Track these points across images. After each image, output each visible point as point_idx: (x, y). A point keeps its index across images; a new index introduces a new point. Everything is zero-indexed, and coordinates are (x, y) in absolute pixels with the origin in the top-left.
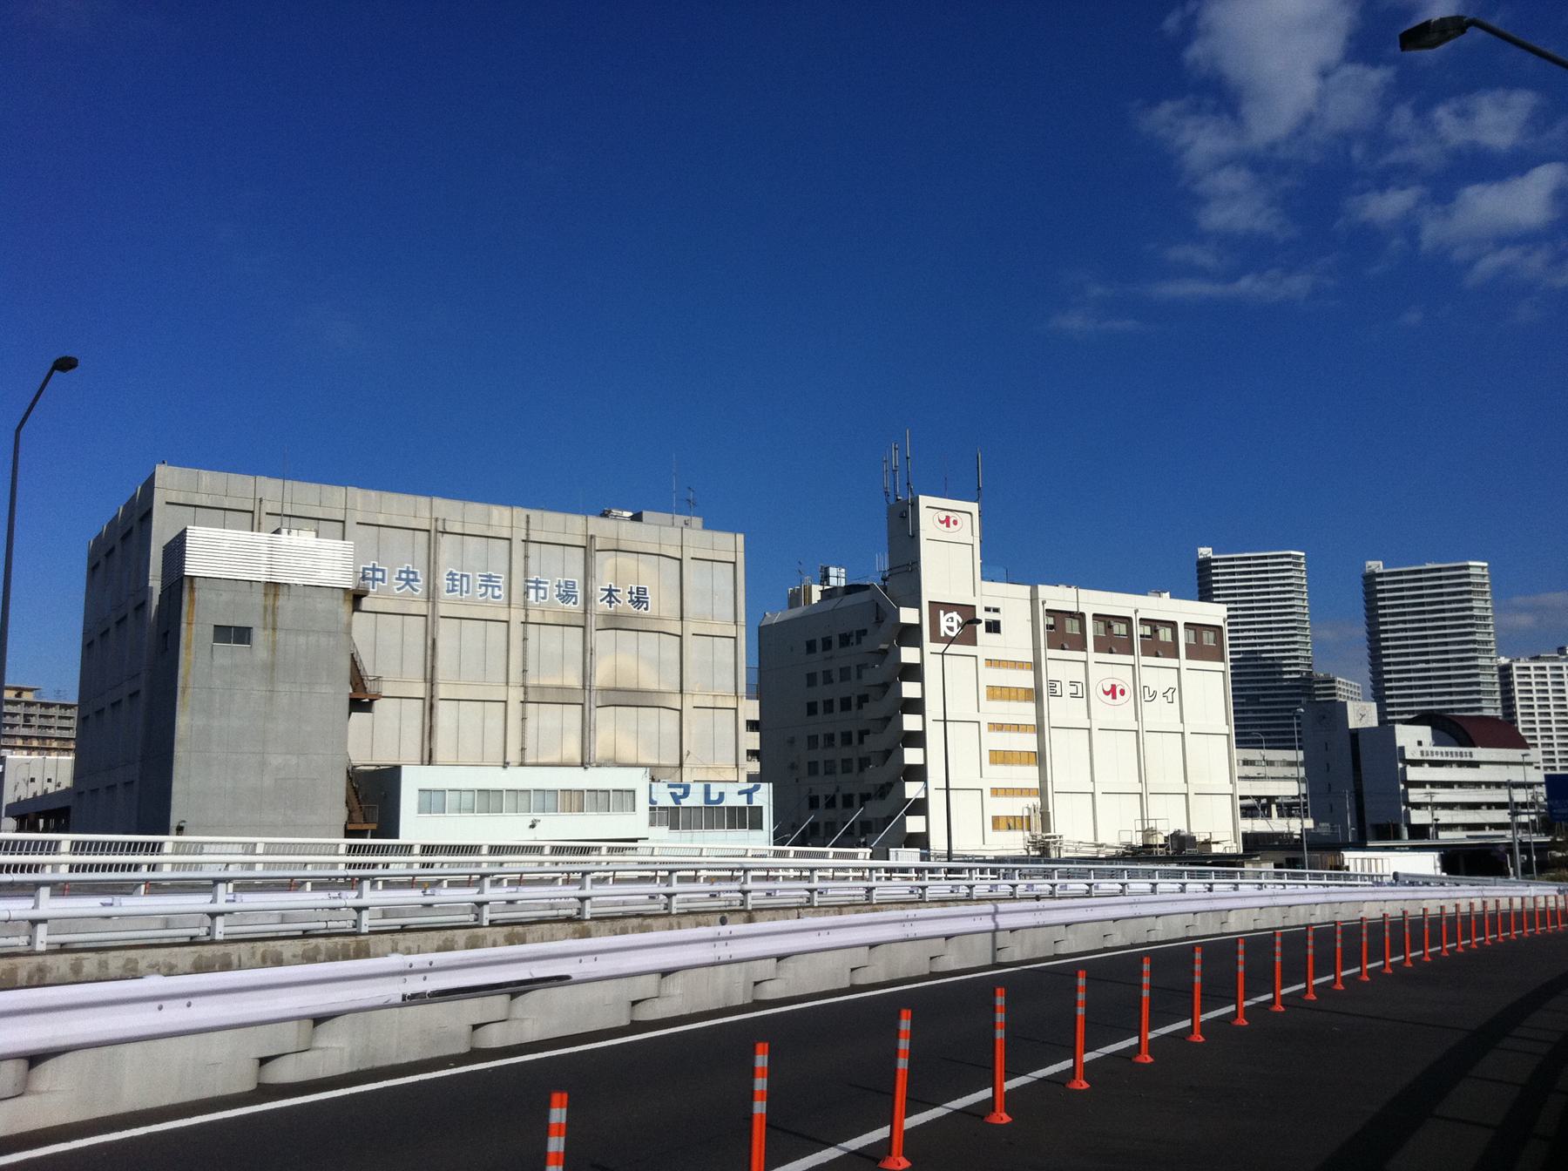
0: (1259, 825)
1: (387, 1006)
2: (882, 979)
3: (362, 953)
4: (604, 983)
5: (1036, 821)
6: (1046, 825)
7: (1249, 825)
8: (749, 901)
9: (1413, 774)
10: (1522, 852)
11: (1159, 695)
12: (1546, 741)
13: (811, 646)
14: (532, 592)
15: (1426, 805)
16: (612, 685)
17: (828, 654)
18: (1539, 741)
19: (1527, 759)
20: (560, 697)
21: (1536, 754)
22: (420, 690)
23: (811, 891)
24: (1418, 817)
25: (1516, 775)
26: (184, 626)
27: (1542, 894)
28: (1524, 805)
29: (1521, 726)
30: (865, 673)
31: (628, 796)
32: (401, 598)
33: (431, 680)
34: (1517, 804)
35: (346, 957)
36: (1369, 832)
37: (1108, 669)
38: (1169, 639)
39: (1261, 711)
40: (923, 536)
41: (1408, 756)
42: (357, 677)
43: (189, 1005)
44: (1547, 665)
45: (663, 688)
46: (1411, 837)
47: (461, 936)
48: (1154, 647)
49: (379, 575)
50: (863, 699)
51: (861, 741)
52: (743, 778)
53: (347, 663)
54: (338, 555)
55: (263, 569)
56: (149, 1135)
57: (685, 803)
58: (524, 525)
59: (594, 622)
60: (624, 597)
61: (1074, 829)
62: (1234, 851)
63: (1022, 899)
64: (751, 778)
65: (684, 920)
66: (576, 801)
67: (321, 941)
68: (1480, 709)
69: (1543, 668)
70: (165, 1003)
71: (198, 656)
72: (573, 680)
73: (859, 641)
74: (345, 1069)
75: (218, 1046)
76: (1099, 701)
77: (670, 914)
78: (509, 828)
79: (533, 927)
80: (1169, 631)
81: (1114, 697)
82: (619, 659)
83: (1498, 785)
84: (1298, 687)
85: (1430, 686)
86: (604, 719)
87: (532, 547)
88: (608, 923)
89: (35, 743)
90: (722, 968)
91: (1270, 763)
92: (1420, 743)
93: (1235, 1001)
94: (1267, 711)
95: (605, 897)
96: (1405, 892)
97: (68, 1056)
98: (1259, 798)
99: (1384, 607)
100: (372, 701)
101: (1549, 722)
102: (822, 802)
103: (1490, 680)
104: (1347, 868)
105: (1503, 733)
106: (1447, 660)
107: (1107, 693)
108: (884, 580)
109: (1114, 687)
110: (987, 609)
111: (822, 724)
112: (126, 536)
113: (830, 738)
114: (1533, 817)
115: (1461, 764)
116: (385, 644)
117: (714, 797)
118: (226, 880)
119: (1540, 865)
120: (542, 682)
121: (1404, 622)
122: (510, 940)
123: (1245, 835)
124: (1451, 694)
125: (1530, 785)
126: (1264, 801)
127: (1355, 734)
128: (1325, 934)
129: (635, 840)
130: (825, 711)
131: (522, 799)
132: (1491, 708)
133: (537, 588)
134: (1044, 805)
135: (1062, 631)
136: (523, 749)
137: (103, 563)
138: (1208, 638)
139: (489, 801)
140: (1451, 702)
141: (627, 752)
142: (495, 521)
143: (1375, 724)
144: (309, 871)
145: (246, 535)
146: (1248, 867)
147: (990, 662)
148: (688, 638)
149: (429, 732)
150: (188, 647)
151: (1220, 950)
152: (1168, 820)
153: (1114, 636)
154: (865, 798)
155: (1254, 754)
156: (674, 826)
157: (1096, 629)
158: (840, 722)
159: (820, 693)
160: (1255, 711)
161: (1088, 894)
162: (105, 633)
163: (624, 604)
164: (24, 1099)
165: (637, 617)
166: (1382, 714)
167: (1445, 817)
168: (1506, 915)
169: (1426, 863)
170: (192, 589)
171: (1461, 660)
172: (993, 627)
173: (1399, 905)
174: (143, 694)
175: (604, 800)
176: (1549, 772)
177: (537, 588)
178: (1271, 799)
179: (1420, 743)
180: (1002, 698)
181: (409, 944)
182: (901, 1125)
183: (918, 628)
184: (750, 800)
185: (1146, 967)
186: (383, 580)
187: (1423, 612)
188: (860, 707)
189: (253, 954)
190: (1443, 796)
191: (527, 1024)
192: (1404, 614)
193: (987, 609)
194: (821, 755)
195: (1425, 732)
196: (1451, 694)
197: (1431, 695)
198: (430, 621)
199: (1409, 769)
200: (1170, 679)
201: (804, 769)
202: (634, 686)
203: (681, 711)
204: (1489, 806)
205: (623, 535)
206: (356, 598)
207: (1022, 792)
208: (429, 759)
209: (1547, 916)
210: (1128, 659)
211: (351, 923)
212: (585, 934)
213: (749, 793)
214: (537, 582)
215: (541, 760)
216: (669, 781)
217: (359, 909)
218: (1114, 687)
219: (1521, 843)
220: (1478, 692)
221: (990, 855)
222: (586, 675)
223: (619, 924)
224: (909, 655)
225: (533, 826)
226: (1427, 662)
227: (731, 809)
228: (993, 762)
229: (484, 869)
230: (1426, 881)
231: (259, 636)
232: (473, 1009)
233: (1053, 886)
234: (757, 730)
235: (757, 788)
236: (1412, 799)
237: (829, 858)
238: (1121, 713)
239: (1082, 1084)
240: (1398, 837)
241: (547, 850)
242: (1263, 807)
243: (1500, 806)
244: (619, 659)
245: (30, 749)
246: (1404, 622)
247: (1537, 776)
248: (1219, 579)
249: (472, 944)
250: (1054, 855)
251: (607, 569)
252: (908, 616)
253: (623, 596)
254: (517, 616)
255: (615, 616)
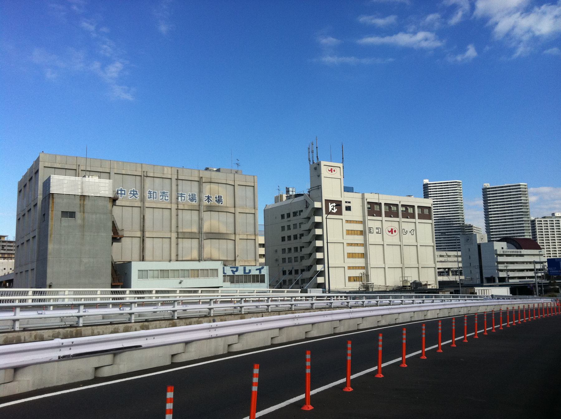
0: (445, 278)
1: (51, 361)
2: (285, 341)
3: (79, 335)
4: (203, 340)
5: (364, 278)
6: (368, 280)
7: (441, 278)
8: (243, 310)
9: (500, 259)
10: (539, 286)
11: (408, 232)
12: (548, 247)
13: (283, 216)
14: (180, 198)
15: (505, 270)
16: (209, 231)
17: (289, 219)
18: (545, 247)
19: (541, 253)
20: (190, 236)
21: (544, 252)
22: (139, 234)
23: (292, 305)
24: (502, 275)
25: (537, 259)
26: (50, 212)
27: (547, 302)
28: (540, 270)
29: (538, 242)
30: (302, 226)
31: (215, 272)
32: (131, 201)
33: (143, 231)
34: (537, 269)
35: (72, 337)
36: (485, 280)
37: (389, 223)
38: (412, 212)
39: (446, 238)
40: (323, 176)
41: (498, 253)
42: (115, 229)
43: (70, 349)
44: (548, 220)
45: (228, 232)
46: (499, 282)
47: (121, 326)
48: (406, 215)
49: (123, 192)
50: (302, 235)
51: (301, 250)
52: (258, 264)
53: (110, 225)
54: (107, 185)
55: (80, 191)
56: (78, 391)
57: (236, 273)
58: (176, 174)
59: (202, 208)
60: (213, 199)
61: (377, 280)
62: (435, 287)
63: (366, 307)
64: (260, 264)
65: (246, 316)
66: (196, 273)
67: (60, 330)
68: (524, 236)
69: (547, 221)
70: (155, 337)
71: (56, 223)
72: (195, 229)
73: (300, 215)
74: (31, 389)
75: (161, 351)
76: (387, 234)
77: (210, 316)
78: (170, 284)
79: (153, 323)
80: (412, 209)
81: (392, 233)
82: (212, 222)
83: (530, 263)
84: (459, 229)
85: (506, 228)
86: (207, 244)
87: (180, 182)
88: (184, 320)
89: (6, 256)
90: (213, 339)
91: (449, 256)
92: (502, 248)
93: (438, 343)
94: (448, 238)
95: (219, 308)
96: (495, 302)
97: (29, 367)
98: (445, 269)
99: (490, 200)
100: (120, 238)
101: (556, 251)
102: (287, 273)
103: (528, 226)
104: (476, 293)
105: (532, 244)
106: (512, 219)
107: (389, 232)
108: (309, 192)
109: (392, 229)
110: (346, 202)
111: (287, 244)
112: (31, 179)
113: (290, 249)
114: (543, 274)
115: (517, 255)
116: (126, 218)
117: (247, 271)
118: (135, 303)
119: (546, 291)
120: (184, 231)
121: (497, 205)
122: (143, 328)
123: (439, 282)
124: (513, 230)
125: (542, 263)
126: (447, 270)
127: (479, 246)
128: (471, 317)
129: (218, 287)
130: (288, 240)
131: (176, 273)
132: (528, 235)
133: (181, 196)
134: (367, 272)
135: (373, 209)
136: (177, 255)
137: (23, 190)
138: (426, 211)
139: (164, 274)
140: (514, 233)
141: (215, 255)
142: (165, 172)
143: (487, 241)
144: (83, 302)
145: (73, 178)
146: (441, 294)
147: (347, 221)
148: (237, 214)
149: (143, 249)
150: (52, 219)
151: (432, 325)
152: (412, 277)
153: (392, 211)
154: (303, 271)
155: (444, 253)
156: (232, 282)
157: (385, 209)
158: (293, 244)
159: (286, 233)
160: (444, 238)
161: (389, 304)
162: (24, 215)
163: (214, 202)
164: (12, 383)
165: (219, 206)
166: (489, 238)
167: (511, 274)
168: (532, 310)
169: (505, 291)
170: (53, 198)
171: (517, 218)
172: (348, 208)
173: (506, 306)
174: (37, 237)
175: (206, 273)
176: (549, 258)
177: (181, 196)
178: (449, 269)
179: (502, 248)
180: (352, 234)
181: (99, 330)
182: (309, 393)
183: (320, 209)
184: (260, 272)
185: (404, 332)
186: (125, 194)
187: (504, 202)
188: (300, 238)
189: (31, 336)
190: (511, 267)
191: (121, 367)
192: (497, 202)
193: (346, 202)
194: (287, 256)
195: (504, 244)
196: (513, 230)
197: (507, 231)
198: (142, 209)
199: (499, 257)
200: (412, 226)
201: (281, 261)
202: (217, 231)
203: (235, 240)
204: (527, 270)
205: (213, 177)
206: (114, 200)
207: (359, 268)
208: (143, 259)
209: (548, 310)
210: (397, 219)
211: (128, 319)
212: (174, 325)
213: (260, 270)
214: (181, 194)
215: (184, 259)
216: (231, 266)
217: (131, 314)
218: (392, 229)
219: (538, 283)
220: (523, 230)
221: (348, 290)
222: (200, 228)
223: (189, 320)
224: (318, 219)
225: (180, 283)
226: (505, 219)
227: (254, 276)
228: (348, 257)
229: (178, 298)
230: (504, 297)
231: (78, 215)
232: (95, 361)
233: (377, 301)
234: (263, 247)
235: (263, 268)
236: (500, 268)
237: (286, 293)
238: (394, 239)
239: (309, 407)
240: (494, 282)
241: (178, 292)
242: (447, 272)
243: (531, 270)
244: (212, 222)
245: (4, 258)
246: (497, 205)
247: (544, 259)
248: (431, 191)
249: (126, 330)
250: (370, 290)
251: (207, 189)
252: (317, 205)
253: (213, 199)
254: (174, 207)
255: (210, 206)
